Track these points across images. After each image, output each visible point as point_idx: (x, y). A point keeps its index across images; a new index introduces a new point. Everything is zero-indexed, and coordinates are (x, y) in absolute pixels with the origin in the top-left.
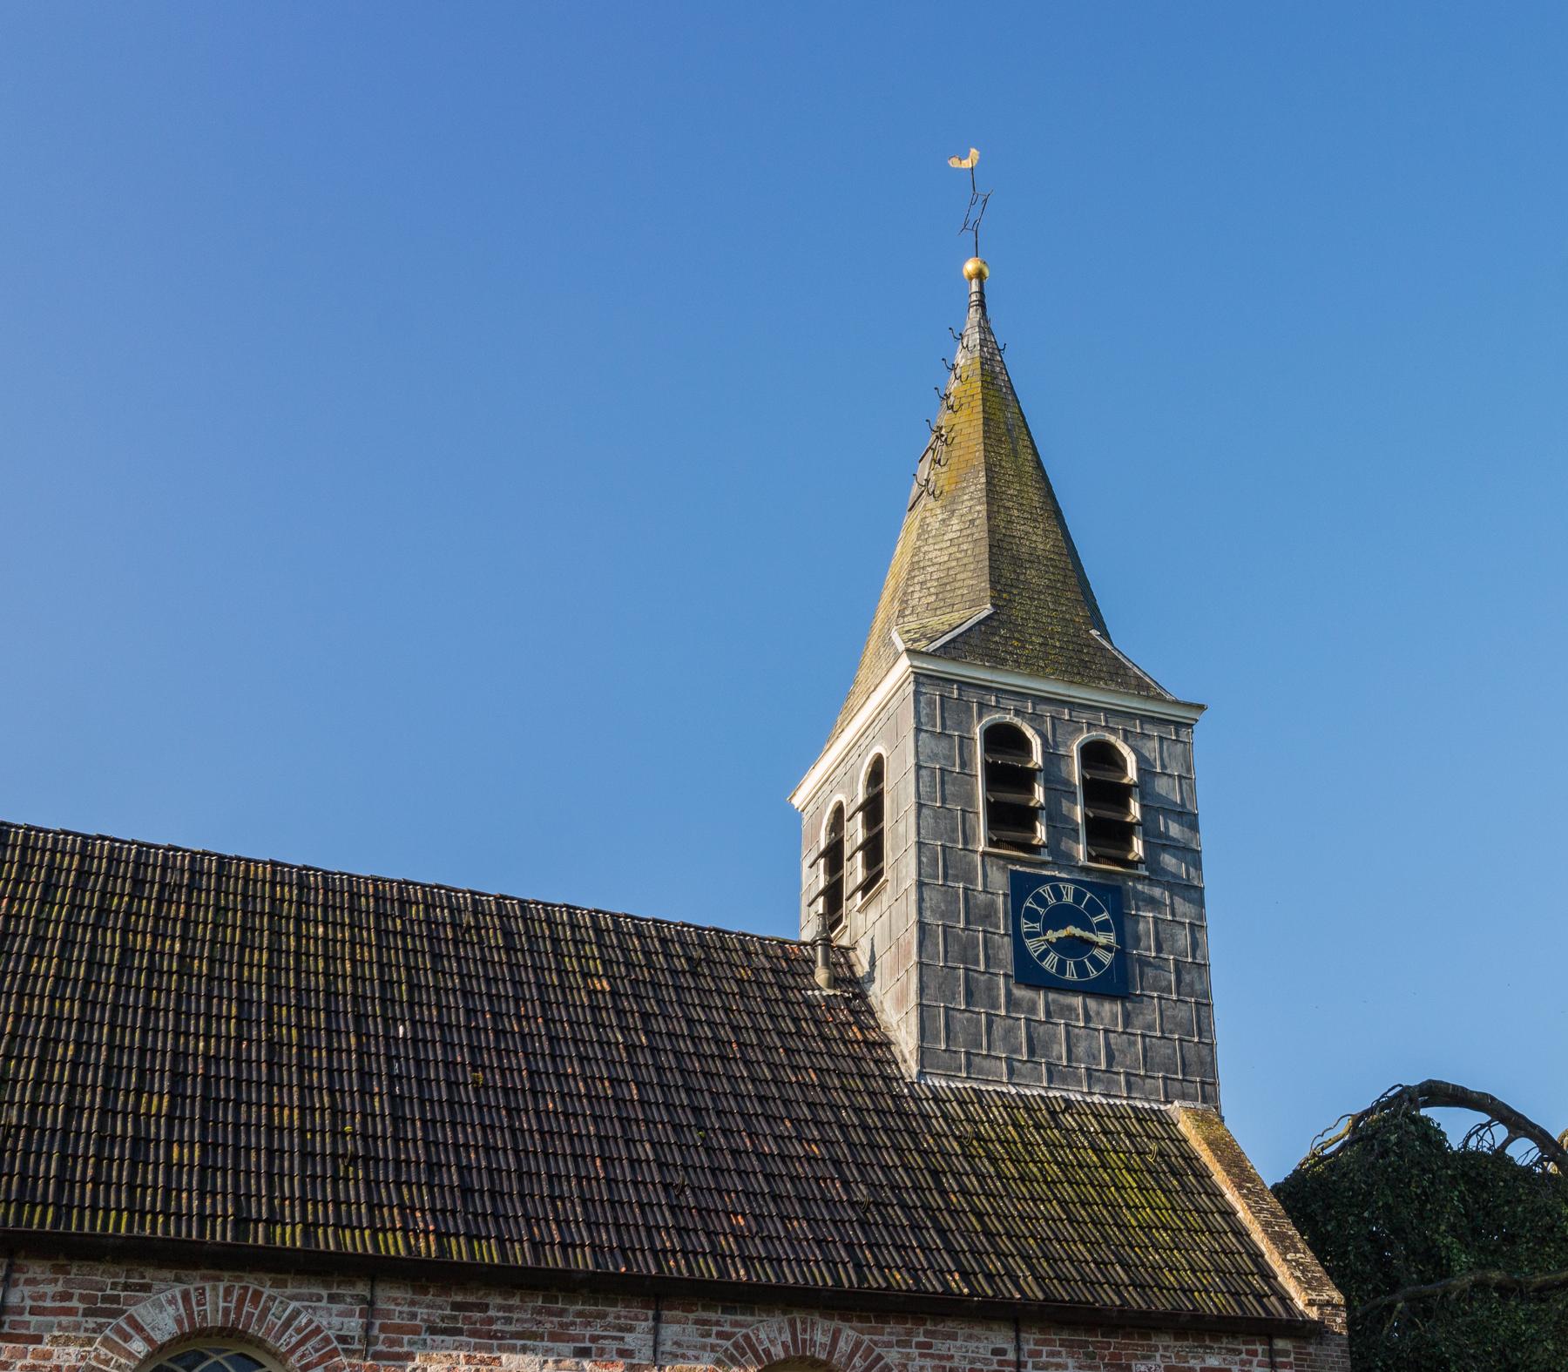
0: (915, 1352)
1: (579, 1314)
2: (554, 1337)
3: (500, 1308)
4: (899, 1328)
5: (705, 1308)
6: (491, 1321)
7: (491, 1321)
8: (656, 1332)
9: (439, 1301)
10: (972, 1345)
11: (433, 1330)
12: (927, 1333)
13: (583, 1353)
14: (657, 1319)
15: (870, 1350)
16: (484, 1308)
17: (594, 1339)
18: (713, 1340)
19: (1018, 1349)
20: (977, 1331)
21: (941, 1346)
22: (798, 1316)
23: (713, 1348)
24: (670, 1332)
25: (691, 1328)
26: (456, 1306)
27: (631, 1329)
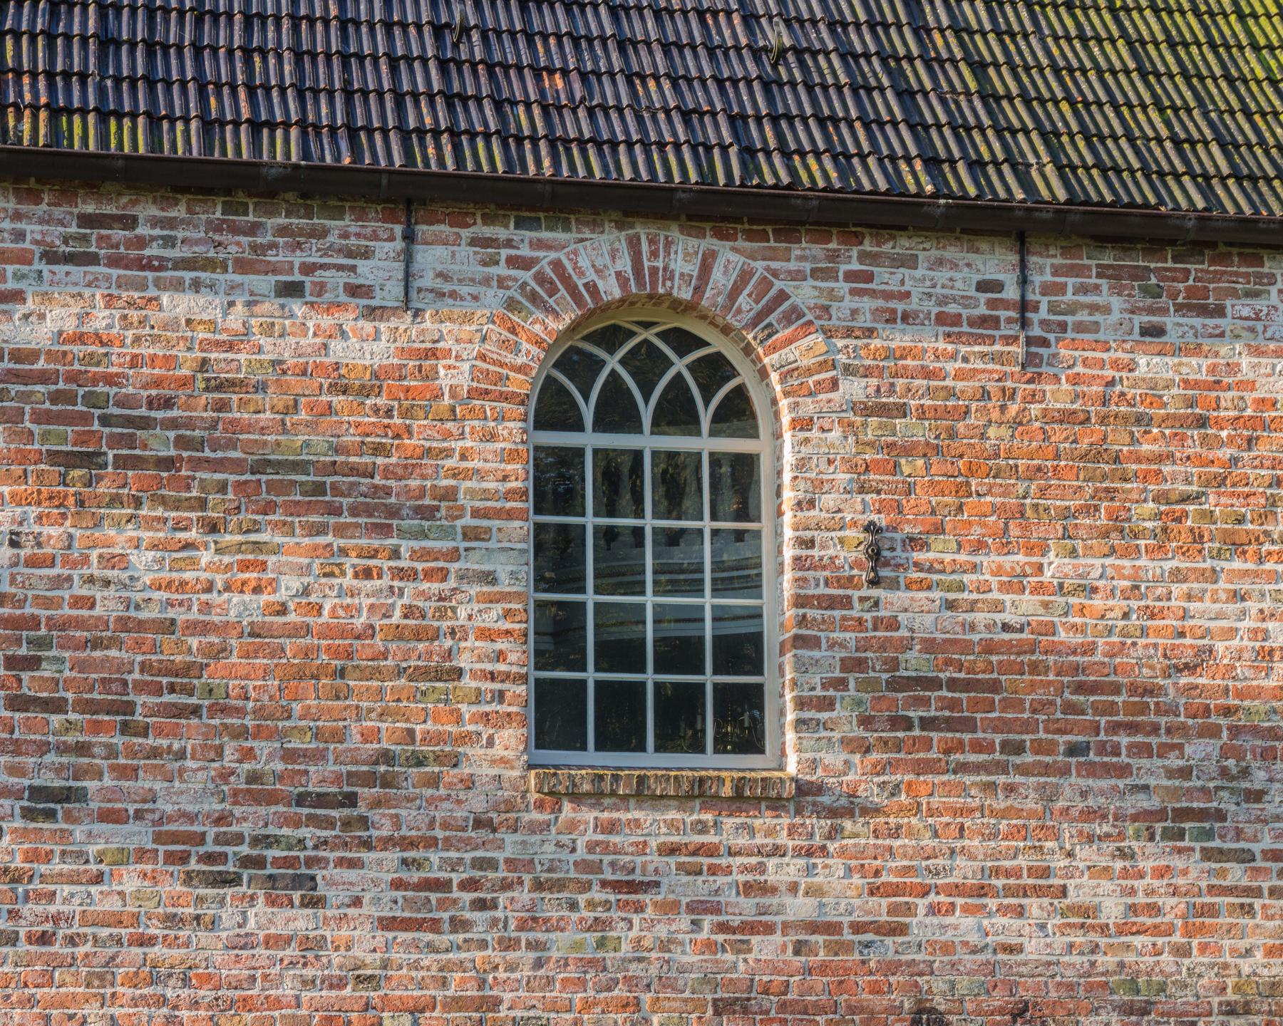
0: (843, 287)
1: (282, 231)
2: (243, 266)
3: (155, 222)
4: (817, 250)
5: (488, 220)
6: (142, 242)
7: (142, 242)
8: (408, 257)
9: (58, 212)
10: (943, 275)
11: (51, 257)
12: (863, 257)
13: (291, 290)
14: (409, 238)
15: (765, 284)
16: (130, 222)
17: (308, 269)
18: (502, 270)
19: (1024, 282)
20: (951, 253)
21: (886, 278)
22: (642, 231)
23: (502, 282)
24: (430, 258)
25: (464, 251)
26: (86, 221)
27: (366, 254)
